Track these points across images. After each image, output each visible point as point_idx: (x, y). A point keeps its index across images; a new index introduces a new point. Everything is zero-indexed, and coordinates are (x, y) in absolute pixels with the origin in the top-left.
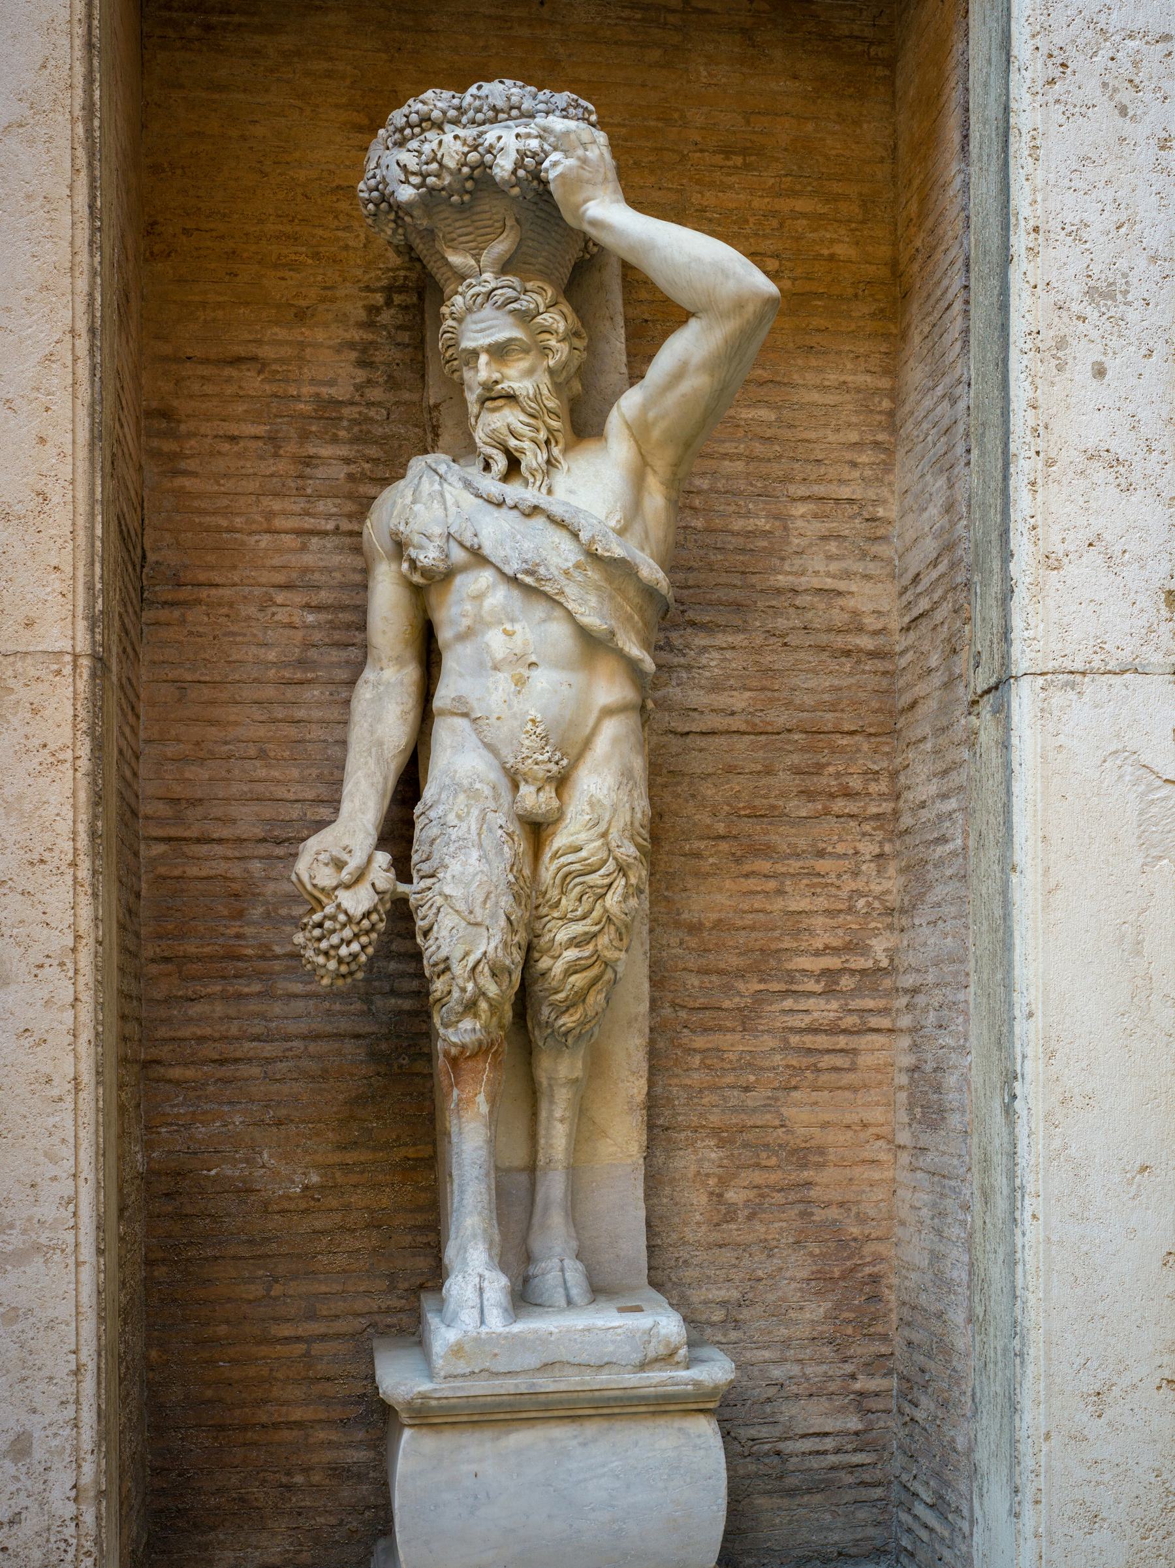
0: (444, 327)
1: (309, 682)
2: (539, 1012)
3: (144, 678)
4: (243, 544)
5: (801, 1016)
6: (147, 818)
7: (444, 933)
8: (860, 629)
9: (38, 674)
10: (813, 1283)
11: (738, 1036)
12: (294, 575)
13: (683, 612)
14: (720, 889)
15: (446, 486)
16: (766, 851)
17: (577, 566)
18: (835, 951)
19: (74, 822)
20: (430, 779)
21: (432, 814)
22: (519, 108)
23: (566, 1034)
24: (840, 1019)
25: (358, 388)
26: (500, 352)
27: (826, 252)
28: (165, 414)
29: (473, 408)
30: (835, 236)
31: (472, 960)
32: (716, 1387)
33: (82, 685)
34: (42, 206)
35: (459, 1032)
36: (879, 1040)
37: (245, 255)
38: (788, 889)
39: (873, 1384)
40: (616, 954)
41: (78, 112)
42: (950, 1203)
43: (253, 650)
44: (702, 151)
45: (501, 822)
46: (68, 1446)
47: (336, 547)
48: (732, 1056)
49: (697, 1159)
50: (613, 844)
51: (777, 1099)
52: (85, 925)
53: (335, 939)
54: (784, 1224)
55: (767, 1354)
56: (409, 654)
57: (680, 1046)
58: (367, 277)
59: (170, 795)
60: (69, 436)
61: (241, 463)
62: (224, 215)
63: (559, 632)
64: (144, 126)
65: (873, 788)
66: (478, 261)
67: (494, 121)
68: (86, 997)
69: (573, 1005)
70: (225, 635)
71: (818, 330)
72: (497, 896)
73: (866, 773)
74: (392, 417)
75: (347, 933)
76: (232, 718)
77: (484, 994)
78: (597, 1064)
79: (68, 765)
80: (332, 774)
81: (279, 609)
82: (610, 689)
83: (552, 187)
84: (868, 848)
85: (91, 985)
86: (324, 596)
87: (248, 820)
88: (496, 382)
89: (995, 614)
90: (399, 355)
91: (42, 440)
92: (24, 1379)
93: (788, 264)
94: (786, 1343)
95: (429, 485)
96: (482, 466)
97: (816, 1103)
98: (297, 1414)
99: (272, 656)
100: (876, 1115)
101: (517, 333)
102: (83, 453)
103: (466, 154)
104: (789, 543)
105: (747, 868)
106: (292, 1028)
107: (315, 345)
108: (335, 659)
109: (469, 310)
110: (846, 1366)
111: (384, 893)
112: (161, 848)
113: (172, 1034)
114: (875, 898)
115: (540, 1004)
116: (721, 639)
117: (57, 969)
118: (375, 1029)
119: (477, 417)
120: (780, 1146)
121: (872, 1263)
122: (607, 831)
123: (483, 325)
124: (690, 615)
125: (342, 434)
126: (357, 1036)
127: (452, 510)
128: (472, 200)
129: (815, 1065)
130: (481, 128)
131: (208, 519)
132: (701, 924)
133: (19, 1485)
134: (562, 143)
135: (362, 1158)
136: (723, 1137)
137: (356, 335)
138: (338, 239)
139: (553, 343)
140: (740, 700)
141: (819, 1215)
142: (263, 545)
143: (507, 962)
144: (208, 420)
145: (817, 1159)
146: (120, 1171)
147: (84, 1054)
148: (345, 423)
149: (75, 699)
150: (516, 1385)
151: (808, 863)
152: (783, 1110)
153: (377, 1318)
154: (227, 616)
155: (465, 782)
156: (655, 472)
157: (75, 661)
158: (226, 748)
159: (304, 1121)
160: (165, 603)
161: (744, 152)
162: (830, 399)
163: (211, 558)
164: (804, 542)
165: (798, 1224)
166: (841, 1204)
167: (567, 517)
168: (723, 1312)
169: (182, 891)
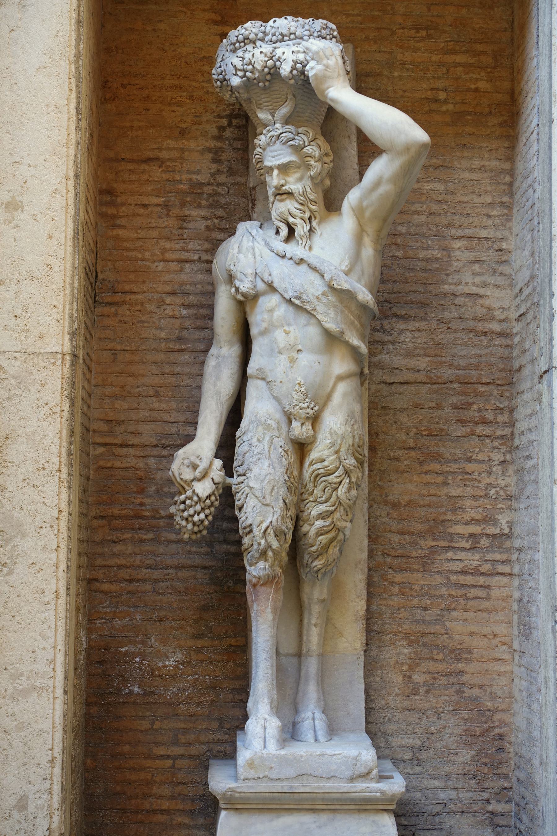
0: (255, 152)
1: (183, 350)
2: (303, 557)
3: (95, 348)
4: (149, 268)
5: (457, 563)
6: (94, 431)
7: (249, 509)
8: (492, 319)
9: (44, 364)
10: (464, 737)
11: (420, 575)
12: (176, 286)
13: (391, 308)
14: (411, 481)
15: (255, 243)
16: (437, 457)
17: (323, 294)
18: (477, 522)
19: (60, 447)
20: (244, 416)
21: (245, 438)
22: (294, 34)
23: (317, 572)
24: (481, 565)
25: (213, 175)
26: (284, 169)
27: (473, 86)
28: (110, 192)
29: (271, 199)
30: (478, 77)
31: (264, 526)
32: (393, 795)
33: (66, 370)
34: (54, 110)
35: (256, 570)
36: (503, 580)
37: (154, 98)
38: (450, 482)
39: (500, 807)
40: (344, 524)
41: (72, 59)
42: (534, 688)
43: (154, 331)
44: (403, 28)
45: (282, 444)
46: (46, 805)
47: (199, 270)
48: (417, 588)
49: (397, 652)
50: (342, 458)
51: (443, 616)
52: (64, 504)
53: (191, 511)
54: (447, 698)
55: (436, 783)
56: (236, 339)
57: (387, 580)
58: (219, 109)
59: (107, 418)
60: (63, 234)
61: (149, 221)
62: (143, 76)
63: (313, 331)
64: (103, 26)
65: (500, 418)
66: (273, 116)
67: (282, 41)
68: (64, 545)
69: (321, 554)
70: (138, 322)
71: (468, 134)
72: (279, 488)
73: (496, 409)
74: (231, 192)
75: (198, 508)
76: (141, 372)
77: (270, 547)
78: (336, 590)
79: (58, 415)
80: (194, 406)
81: (168, 307)
82: (341, 365)
83: (310, 79)
84: (497, 457)
85: (66, 539)
86: (192, 299)
87: (148, 433)
88: (282, 186)
89: (547, 326)
90: (235, 155)
91: (50, 236)
92: (25, 764)
93: (452, 95)
94: (448, 776)
95: (247, 243)
96: (275, 231)
97: (466, 620)
98: (166, 805)
99: (163, 335)
100: (501, 629)
101: (293, 158)
102: (70, 243)
103: (266, 62)
104: (451, 265)
105: (426, 468)
106: (169, 561)
107: (190, 150)
108: (196, 337)
109: (268, 144)
110: (484, 794)
111: (218, 484)
112: (101, 450)
113: (104, 563)
114: (501, 488)
115: (304, 553)
116: (413, 325)
117: (49, 529)
118: (214, 563)
119: (273, 203)
120: (445, 646)
121: (499, 726)
122: (339, 449)
123: (275, 153)
124: (395, 310)
125: (204, 202)
126: (205, 568)
127: (258, 258)
128: (270, 84)
129: (465, 595)
130: (275, 45)
131: (131, 253)
132: (399, 502)
133: (21, 826)
134: (317, 57)
135: (206, 644)
136: (412, 639)
137: (212, 144)
138: (203, 88)
139: (312, 163)
140: (423, 363)
141: (468, 693)
142: (160, 269)
143: (284, 528)
144: (132, 195)
145: (466, 656)
146: (76, 645)
147: (61, 578)
148: (205, 196)
149: (62, 378)
150: (282, 787)
151: (462, 466)
152: (447, 623)
153: (212, 746)
154: (140, 311)
155: (263, 419)
156: (368, 235)
157: (63, 357)
158: (138, 390)
159: (174, 620)
160: (107, 303)
161: (427, 28)
162: (475, 176)
163: (132, 277)
164: (460, 264)
165: (455, 698)
166: (481, 687)
167: (318, 265)
168: (411, 753)
169: (112, 476)
